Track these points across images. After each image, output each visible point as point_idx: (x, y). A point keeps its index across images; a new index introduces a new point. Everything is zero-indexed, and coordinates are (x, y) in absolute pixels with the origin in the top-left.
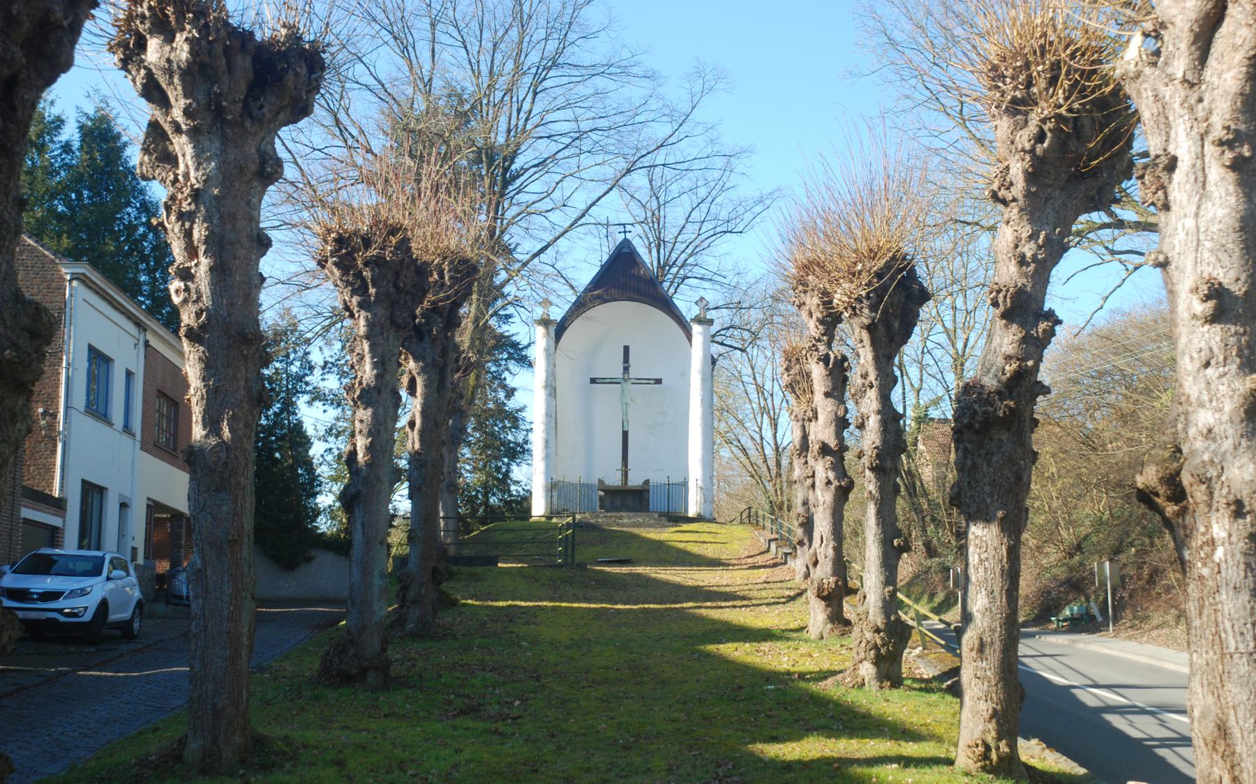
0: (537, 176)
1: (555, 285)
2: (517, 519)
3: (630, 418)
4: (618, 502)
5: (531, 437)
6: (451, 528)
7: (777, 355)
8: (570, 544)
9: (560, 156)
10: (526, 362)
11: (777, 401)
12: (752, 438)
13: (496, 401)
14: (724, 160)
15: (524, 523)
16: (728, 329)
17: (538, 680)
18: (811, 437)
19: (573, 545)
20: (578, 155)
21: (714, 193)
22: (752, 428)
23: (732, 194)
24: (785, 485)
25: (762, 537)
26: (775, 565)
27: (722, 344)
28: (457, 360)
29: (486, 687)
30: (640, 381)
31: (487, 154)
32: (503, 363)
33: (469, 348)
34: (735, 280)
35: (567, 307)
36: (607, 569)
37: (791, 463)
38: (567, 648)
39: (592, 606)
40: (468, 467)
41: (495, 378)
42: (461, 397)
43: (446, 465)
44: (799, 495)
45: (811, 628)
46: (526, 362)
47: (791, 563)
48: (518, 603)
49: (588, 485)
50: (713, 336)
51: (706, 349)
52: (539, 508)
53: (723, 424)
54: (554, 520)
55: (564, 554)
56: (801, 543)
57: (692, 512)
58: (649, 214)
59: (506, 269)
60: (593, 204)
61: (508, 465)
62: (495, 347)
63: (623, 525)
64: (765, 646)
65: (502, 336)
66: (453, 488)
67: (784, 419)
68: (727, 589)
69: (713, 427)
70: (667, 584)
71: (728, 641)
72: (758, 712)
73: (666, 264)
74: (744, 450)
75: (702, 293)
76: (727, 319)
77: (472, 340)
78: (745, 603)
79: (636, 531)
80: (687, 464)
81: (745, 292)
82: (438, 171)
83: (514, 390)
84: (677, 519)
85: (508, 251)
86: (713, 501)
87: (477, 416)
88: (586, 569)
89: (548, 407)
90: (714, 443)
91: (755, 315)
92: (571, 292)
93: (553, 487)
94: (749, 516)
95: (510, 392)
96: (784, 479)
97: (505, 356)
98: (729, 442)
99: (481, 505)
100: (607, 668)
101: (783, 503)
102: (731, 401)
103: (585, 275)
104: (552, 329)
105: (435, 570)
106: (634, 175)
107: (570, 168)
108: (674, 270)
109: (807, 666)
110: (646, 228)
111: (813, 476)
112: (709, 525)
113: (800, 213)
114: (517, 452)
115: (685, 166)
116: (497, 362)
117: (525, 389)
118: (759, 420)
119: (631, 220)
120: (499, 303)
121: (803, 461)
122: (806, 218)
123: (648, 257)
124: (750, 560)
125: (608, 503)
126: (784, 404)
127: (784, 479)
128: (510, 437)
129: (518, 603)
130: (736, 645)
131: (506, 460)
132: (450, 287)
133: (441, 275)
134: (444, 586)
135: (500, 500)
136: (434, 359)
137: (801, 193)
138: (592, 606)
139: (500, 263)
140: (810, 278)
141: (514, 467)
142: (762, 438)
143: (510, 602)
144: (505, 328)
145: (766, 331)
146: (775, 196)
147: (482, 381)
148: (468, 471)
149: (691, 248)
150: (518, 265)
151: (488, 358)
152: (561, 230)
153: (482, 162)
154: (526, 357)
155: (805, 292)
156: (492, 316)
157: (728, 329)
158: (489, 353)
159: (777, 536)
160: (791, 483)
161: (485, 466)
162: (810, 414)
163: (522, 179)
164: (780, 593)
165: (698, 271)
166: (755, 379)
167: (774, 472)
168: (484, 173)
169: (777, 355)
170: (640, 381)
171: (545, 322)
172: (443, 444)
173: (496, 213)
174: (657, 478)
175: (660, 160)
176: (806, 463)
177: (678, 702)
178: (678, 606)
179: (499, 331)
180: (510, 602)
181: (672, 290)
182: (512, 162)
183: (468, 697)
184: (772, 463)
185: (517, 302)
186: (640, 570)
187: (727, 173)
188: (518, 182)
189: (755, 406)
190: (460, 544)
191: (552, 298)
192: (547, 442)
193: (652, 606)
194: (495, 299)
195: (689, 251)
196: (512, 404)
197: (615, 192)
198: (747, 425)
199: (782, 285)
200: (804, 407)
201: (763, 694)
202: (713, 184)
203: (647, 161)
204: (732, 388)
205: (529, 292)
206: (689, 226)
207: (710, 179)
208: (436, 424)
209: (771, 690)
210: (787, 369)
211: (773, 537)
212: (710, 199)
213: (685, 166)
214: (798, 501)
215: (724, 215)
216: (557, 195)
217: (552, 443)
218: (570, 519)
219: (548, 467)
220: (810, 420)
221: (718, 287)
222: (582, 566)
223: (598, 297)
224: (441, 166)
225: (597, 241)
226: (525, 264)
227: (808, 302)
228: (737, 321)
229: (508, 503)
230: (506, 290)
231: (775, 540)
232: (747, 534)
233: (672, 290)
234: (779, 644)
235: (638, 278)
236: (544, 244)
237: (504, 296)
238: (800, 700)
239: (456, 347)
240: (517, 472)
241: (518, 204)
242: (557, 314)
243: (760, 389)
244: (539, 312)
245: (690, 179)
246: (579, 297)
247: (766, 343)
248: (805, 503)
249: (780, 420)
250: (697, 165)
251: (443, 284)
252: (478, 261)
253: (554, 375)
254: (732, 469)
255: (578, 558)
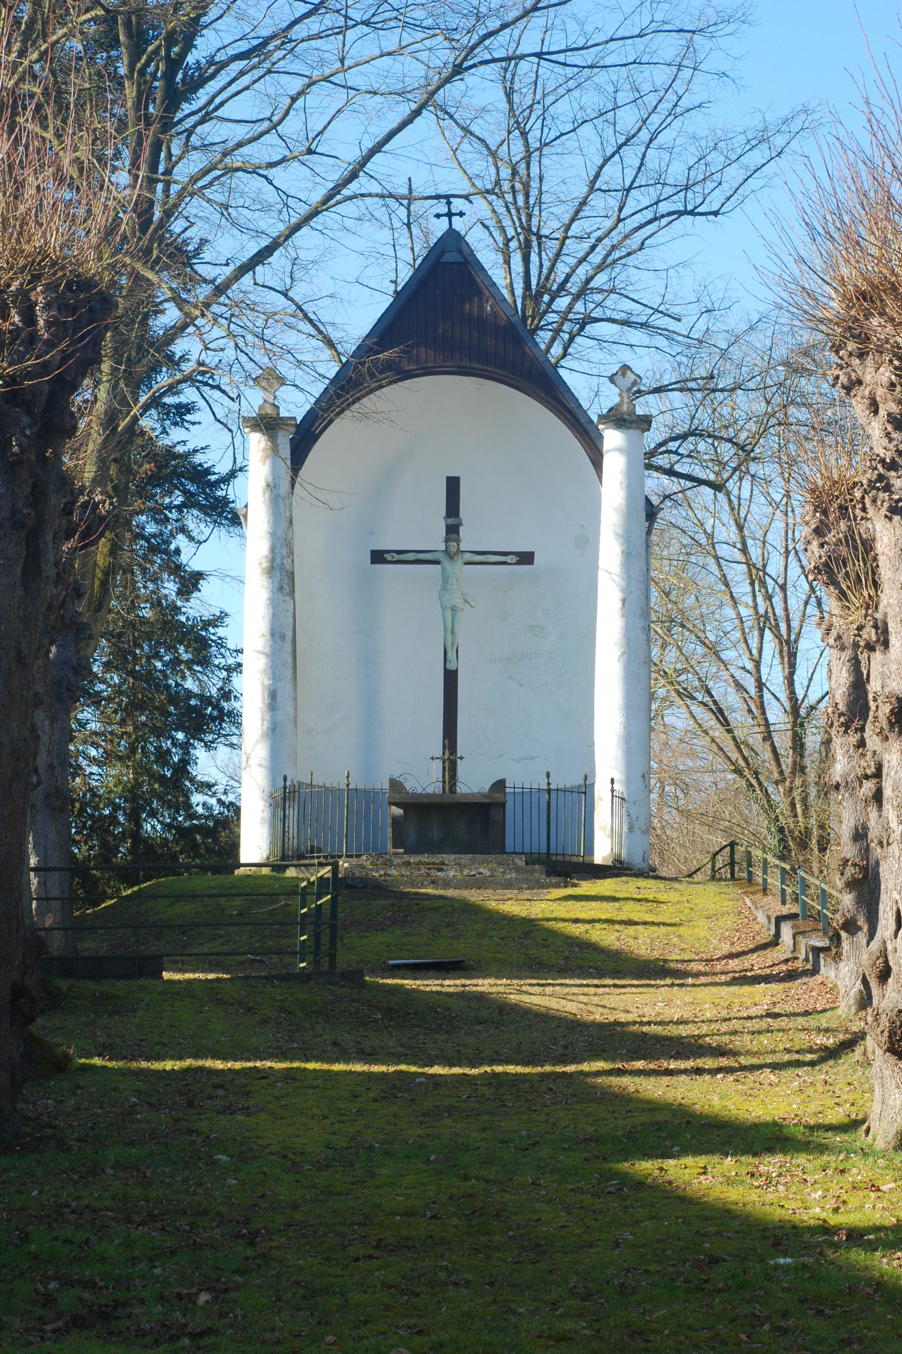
0: (245, 80)
1: (290, 339)
2: (204, 869)
3: (461, 640)
4: (436, 833)
5: (238, 683)
6: (54, 892)
7: (797, 498)
8: (327, 926)
9: (299, 32)
10: (226, 515)
11: (795, 604)
12: (739, 686)
13: (156, 604)
14: (679, 40)
15: (220, 879)
16: (684, 437)
17: (252, 1244)
18: (874, 686)
19: (333, 928)
20: (342, 31)
21: (655, 120)
22: (738, 661)
23: (696, 123)
24: (813, 791)
25: (763, 911)
26: (791, 976)
27: (670, 472)
28: (67, 511)
29: (134, 1261)
30: (483, 558)
31: (128, 24)
32: (173, 515)
33: (95, 482)
34: (701, 325)
35: (318, 389)
36: (409, 983)
37: (827, 742)
38: (321, 1166)
39: (376, 1068)
40: (93, 752)
41: (154, 549)
42: (78, 593)
43: (43, 749)
44: (845, 817)
45: (874, 1124)
46: (226, 515)
47: (827, 971)
48: (208, 1063)
49: (367, 792)
50: (651, 454)
51: (633, 484)
52: (254, 845)
53: (672, 654)
54: (291, 873)
55: (314, 950)
56: (850, 926)
57: (602, 853)
58: (505, 173)
59: (180, 303)
60: (377, 148)
61: (186, 747)
62: (154, 480)
63: (447, 884)
64: (771, 1164)
65: (170, 453)
66: (60, 801)
67: (811, 643)
68: (683, 1031)
69: (648, 661)
70: (544, 1018)
71: (685, 1151)
72: (756, 1320)
73: (543, 288)
74: (720, 713)
75: (626, 356)
76: (684, 414)
77: (102, 464)
78: (724, 1062)
79: (474, 896)
80: (591, 745)
81: (724, 353)
82: (15, 66)
83: (198, 576)
84: (568, 867)
85: (181, 257)
86: (648, 829)
87: (115, 637)
88: (364, 984)
89: (275, 617)
90: (652, 697)
91: (747, 405)
92: (327, 353)
93: (286, 798)
94: (732, 863)
95: (191, 583)
96: (812, 776)
97: (178, 499)
98: (686, 695)
99: (123, 837)
100: (409, 1213)
101: (808, 832)
102: (690, 601)
103: (358, 314)
104: (285, 439)
105: (18, 991)
106: (471, 79)
107: (322, 62)
108: (562, 303)
109: (866, 1212)
110: (499, 205)
111: (878, 774)
112: (641, 882)
113: (851, 166)
114: (209, 718)
115: (589, 56)
116: (159, 514)
117: (224, 576)
118: (754, 643)
119: (464, 187)
120: (163, 379)
121: (853, 738)
122: (868, 184)
123: (502, 273)
124: (733, 964)
125: (411, 832)
126: (812, 610)
127: (812, 776)
128: (190, 684)
129: (208, 1063)
130: (702, 1160)
131: (180, 736)
132: (50, 344)
133: (29, 317)
134: (40, 1025)
135: (167, 827)
136: (14, 511)
137: (856, 123)
138: (376, 1068)
139: (164, 285)
140: (875, 321)
141: (199, 752)
142: (760, 685)
143: (188, 1062)
144: (176, 434)
145: (771, 442)
146: (795, 126)
147: (125, 558)
148: (93, 761)
149: (601, 251)
150: (203, 292)
151: (138, 504)
152: (303, 210)
153: (115, 43)
154: (225, 502)
155: (862, 355)
156: (146, 408)
157: (684, 437)
158: (142, 493)
159: (795, 909)
160: (828, 789)
161: (133, 750)
162: (869, 634)
163: (212, 87)
164: (801, 1040)
165: (618, 306)
166: (744, 550)
167: (787, 763)
168: (123, 70)
169: (797, 498)
170: (483, 558)
171: (267, 423)
172: (37, 702)
173: (153, 167)
174: (523, 776)
175: (530, 44)
176: (862, 744)
177: (572, 1292)
178: (571, 1068)
179: (166, 441)
180: (188, 1062)
181: (557, 350)
182: (189, 46)
183: (90, 1285)
184: (783, 742)
185: (202, 377)
186: (484, 985)
187: (686, 73)
188: (203, 95)
189: (744, 612)
190: (74, 929)
191: (285, 368)
192: (273, 695)
193: (511, 1069)
194: (155, 369)
195: (596, 258)
196: (194, 609)
197: (427, 119)
198: (728, 655)
199: (807, 337)
200: (857, 616)
201: (767, 1277)
202: (652, 99)
203: (499, 46)
204: (692, 570)
205: (230, 353)
206: (597, 201)
207: (646, 87)
208: (20, 658)
209: (786, 1269)
210: (819, 532)
211: (785, 910)
212: (644, 135)
213: (589, 56)
214: (844, 829)
215: (677, 172)
216: (292, 126)
217: (284, 697)
218: (325, 872)
219: (275, 754)
220: (870, 648)
221: (661, 342)
222: (354, 977)
223: (389, 366)
224: (22, 53)
225: (385, 235)
226: (221, 290)
227: (868, 378)
228: (704, 419)
229: (183, 833)
230: (179, 347)
231: (793, 917)
232: (727, 904)
233: (557, 350)
234: (801, 1159)
235: (481, 324)
236: (265, 242)
237: (173, 362)
238: (852, 1291)
239: (66, 481)
240: (206, 764)
241: (205, 147)
242: (295, 404)
243: (757, 575)
244: (254, 400)
245: (599, 88)
246: (344, 366)
247: (769, 469)
248: (860, 835)
249: (803, 645)
250: (616, 54)
251: (33, 338)
252: (113, 283)
253: (288, 544)
254: (692, 754)
255: (344, 959)
